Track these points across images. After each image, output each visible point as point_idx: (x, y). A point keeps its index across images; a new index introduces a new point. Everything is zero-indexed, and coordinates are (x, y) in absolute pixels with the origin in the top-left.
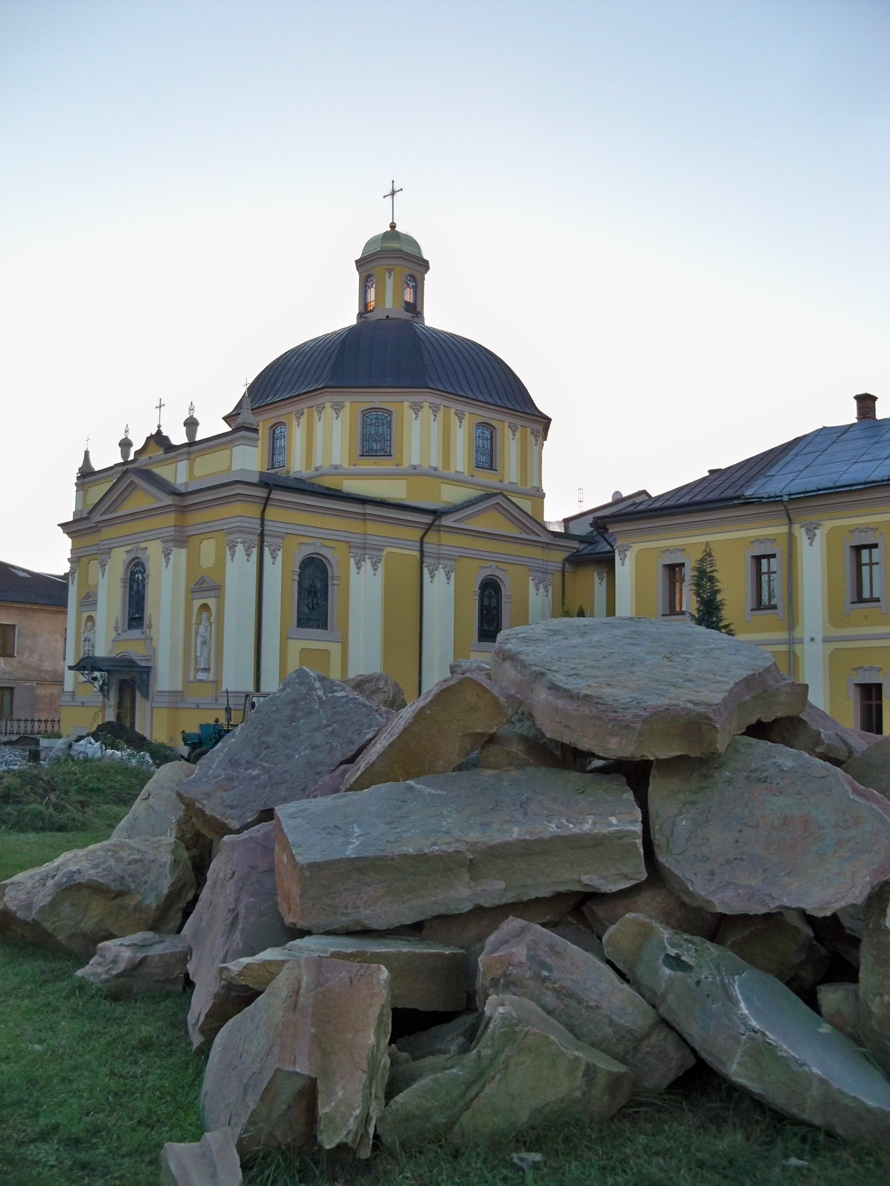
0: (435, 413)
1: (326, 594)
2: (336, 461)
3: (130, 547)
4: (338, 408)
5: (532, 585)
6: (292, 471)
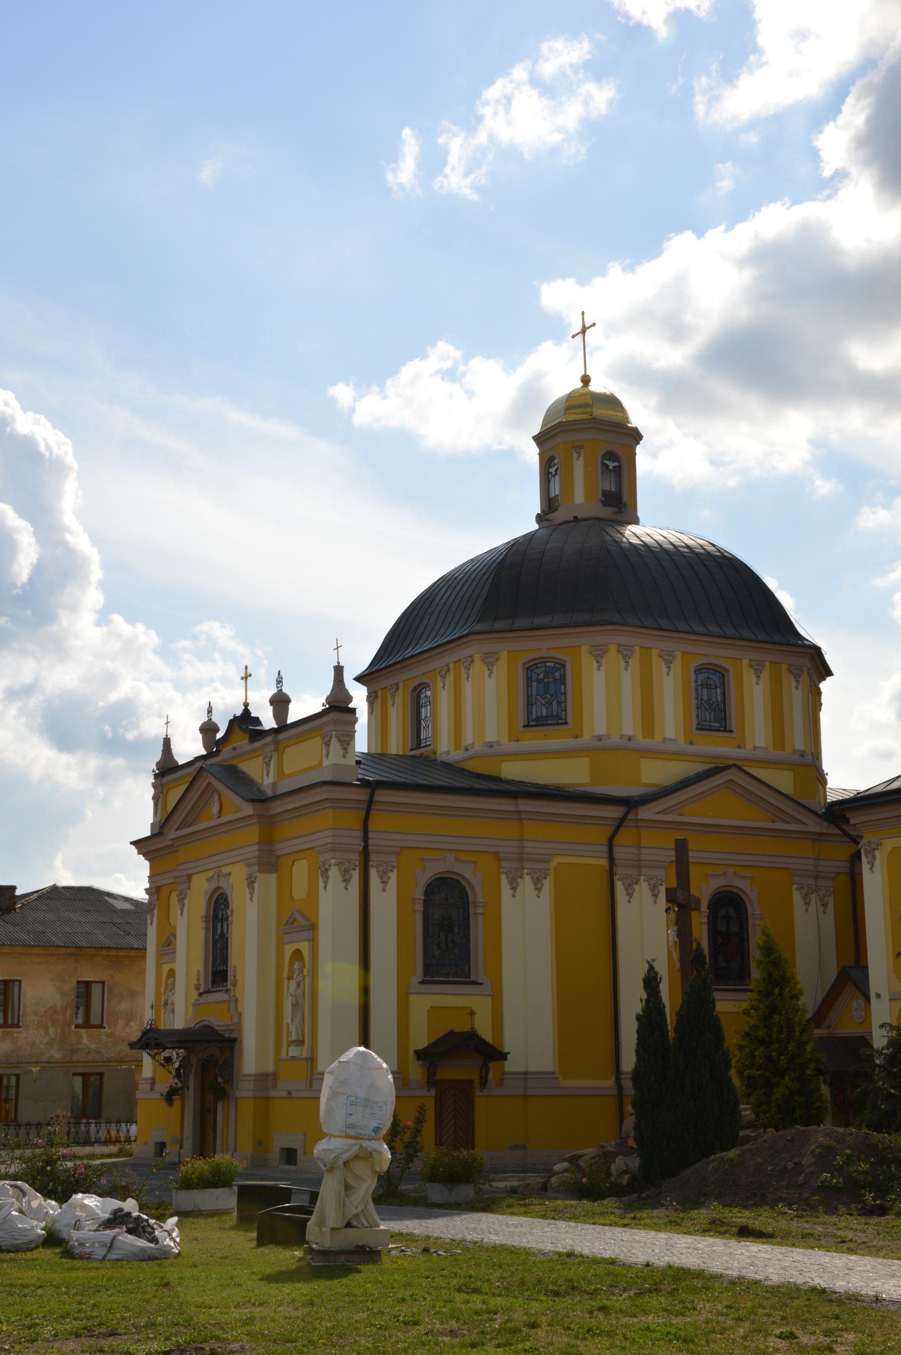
0: (627, 658)
1: (467, 928)
2: (491, 736)
3: (210, 874)
4: (490, 661)
5: (797, 897)
6: (439, 752)
